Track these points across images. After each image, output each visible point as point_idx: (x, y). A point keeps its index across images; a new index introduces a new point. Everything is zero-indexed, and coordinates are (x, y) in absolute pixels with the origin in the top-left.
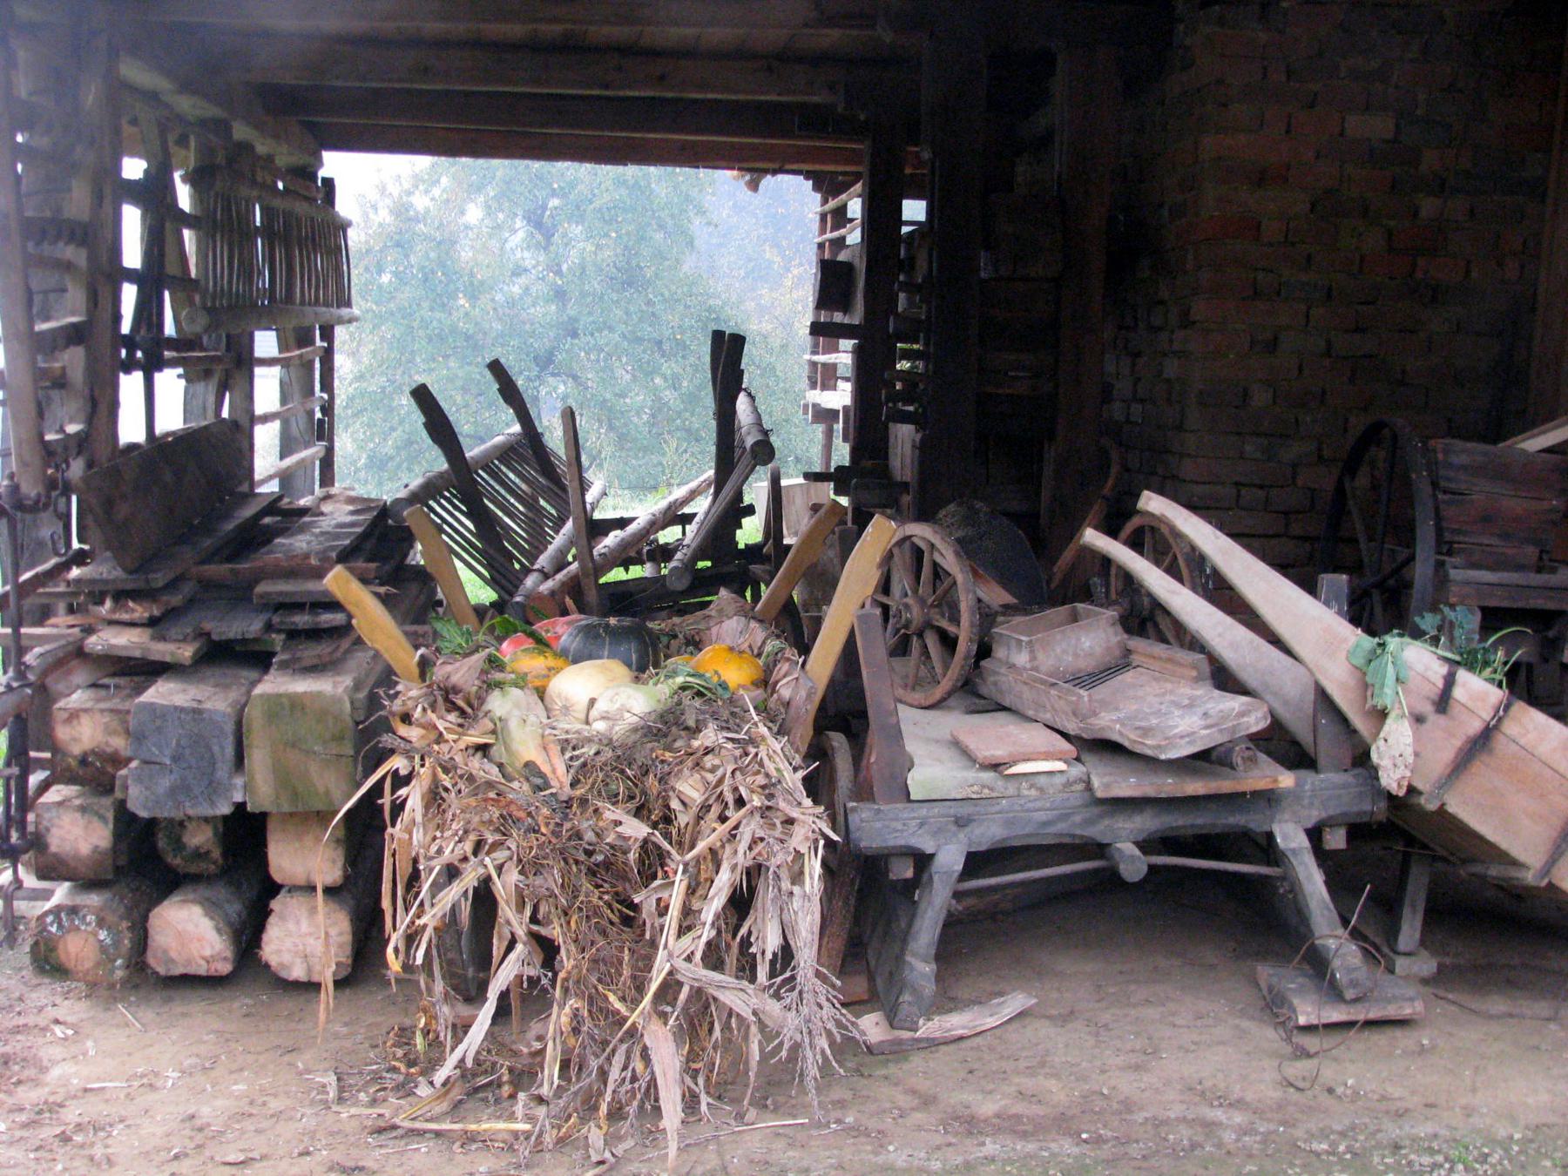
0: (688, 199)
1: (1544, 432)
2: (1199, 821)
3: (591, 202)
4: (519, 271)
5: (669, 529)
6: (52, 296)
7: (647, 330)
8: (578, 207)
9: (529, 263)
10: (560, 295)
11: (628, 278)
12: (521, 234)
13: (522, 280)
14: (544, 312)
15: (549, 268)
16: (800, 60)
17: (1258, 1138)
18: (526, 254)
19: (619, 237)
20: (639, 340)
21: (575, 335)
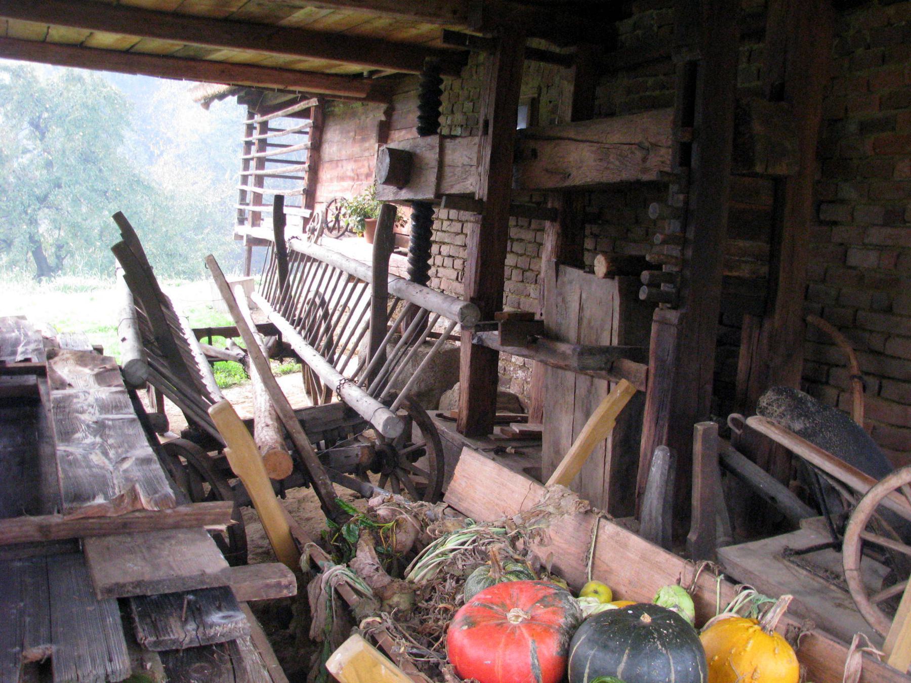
0: (121, 117)
1: (476, 272)
2: (654, 489)
3: (67, 116)
4: (25, 151)
5: (236, 295)
6: (538, 233)
7: (100, 186)
8: (60, 118)
9: (30, 148)
10: (49, 165)
11: (87, 158)
12: (27, 131)
13: (28, 155)
14: (39, 174)
15: (44, 151)
16: (231, 21)
17: (865, 649)
18: (29, 142)
19: (84, 135)
20: (95, 191)
21: (60, 187)
